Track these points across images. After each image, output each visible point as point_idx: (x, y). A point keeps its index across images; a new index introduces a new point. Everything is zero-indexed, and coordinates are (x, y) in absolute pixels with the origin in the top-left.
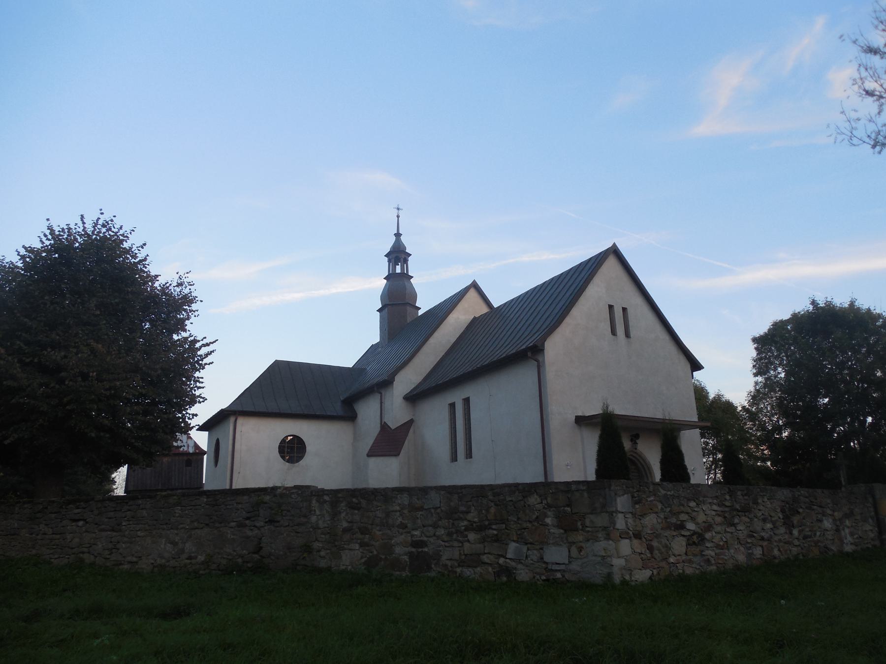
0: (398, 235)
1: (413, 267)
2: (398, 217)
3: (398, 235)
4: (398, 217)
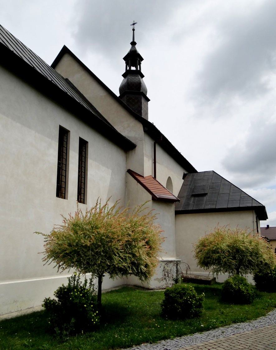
0: (133, 44)
1: (144, 67)
2: (134, 30)
3: (133, 44)
4: (134, 30)
